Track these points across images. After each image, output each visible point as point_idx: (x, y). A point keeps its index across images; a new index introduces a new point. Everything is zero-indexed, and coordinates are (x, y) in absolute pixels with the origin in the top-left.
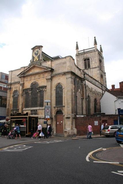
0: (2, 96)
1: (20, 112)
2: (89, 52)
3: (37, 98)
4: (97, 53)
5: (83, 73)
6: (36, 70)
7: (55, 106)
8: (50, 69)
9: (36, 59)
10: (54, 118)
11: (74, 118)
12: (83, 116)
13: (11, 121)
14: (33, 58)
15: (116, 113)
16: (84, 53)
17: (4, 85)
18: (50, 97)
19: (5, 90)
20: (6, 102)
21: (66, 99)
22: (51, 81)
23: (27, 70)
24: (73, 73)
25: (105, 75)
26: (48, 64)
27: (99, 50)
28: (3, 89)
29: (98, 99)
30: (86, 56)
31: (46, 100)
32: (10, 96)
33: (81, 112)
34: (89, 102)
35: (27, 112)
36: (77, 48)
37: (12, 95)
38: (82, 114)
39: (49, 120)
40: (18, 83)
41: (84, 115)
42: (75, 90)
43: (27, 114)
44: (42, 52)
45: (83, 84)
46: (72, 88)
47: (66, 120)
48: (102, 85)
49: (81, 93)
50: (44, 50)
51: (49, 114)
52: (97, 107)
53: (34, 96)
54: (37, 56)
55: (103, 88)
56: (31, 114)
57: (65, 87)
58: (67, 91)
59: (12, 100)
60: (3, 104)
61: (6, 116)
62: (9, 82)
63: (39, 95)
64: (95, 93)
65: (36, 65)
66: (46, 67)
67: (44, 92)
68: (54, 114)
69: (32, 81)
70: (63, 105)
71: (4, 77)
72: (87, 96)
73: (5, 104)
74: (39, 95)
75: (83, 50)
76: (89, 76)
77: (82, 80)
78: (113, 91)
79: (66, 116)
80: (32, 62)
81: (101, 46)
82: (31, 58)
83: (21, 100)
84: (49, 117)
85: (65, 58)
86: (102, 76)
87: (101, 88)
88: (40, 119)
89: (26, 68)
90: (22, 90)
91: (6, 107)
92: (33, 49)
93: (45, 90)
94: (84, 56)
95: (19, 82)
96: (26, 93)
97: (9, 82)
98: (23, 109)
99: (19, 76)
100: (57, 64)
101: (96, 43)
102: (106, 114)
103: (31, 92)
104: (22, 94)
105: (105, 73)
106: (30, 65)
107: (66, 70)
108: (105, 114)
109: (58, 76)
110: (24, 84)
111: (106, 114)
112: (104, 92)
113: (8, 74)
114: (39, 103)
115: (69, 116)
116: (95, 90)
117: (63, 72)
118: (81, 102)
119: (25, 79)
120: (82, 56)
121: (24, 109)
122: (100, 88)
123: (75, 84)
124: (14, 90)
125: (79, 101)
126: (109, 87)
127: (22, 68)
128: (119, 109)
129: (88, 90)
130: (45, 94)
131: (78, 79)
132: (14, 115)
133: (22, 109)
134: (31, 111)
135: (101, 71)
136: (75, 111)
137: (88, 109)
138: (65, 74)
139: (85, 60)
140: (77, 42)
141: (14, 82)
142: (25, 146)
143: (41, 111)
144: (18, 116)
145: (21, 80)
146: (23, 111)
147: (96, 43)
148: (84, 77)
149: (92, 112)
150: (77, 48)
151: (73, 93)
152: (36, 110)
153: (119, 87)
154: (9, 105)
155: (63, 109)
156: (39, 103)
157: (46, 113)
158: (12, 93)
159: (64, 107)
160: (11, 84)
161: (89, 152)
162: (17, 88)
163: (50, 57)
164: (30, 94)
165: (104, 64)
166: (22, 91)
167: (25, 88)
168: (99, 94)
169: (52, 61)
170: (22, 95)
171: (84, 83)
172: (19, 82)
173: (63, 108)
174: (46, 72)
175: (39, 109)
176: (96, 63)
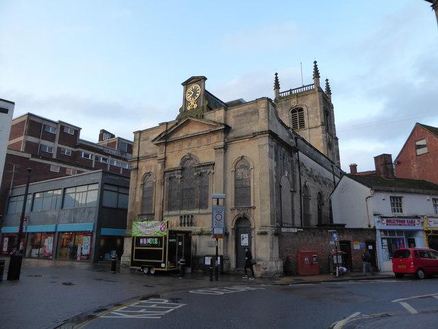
10: (230, 234)
12: (296, 230)
14: (186, 102)
25: (337, 144)
27: (324, 90)
28: (121, 173)
29: (326, 190)
34: (305, 198)
38: (294, 227)
41: (298, 228)
51: (222, 224)
52: (323, 211)
53: (187, 186)
66: (214, 122)
69: (184, 153)
70: (252, 205)
77: (292, 150)
78: (354, 175)
79: (257, 230)
80: (183, 111)
82: (180, 104)
85: (257, 101)
87: (331, 169)
89: (170, 126)
92: (187, 84)
101: (316, 74)
106: (179, 118)
110: (165, 158)
112: (337, 179)
118: (290, 199)
123: (276, 159)
127: (161, 124)
129: (304, 173)
137: (305, 217)
143: (202, 217)
145: (161, 150)
147: (316, 74)
149: (314, 221)
153: (374, 169)
159: (254, 208)
165: (334, 120)
167: (167, 169)
174: (214, 132)
175: (199, 214)
176: (317, 117)
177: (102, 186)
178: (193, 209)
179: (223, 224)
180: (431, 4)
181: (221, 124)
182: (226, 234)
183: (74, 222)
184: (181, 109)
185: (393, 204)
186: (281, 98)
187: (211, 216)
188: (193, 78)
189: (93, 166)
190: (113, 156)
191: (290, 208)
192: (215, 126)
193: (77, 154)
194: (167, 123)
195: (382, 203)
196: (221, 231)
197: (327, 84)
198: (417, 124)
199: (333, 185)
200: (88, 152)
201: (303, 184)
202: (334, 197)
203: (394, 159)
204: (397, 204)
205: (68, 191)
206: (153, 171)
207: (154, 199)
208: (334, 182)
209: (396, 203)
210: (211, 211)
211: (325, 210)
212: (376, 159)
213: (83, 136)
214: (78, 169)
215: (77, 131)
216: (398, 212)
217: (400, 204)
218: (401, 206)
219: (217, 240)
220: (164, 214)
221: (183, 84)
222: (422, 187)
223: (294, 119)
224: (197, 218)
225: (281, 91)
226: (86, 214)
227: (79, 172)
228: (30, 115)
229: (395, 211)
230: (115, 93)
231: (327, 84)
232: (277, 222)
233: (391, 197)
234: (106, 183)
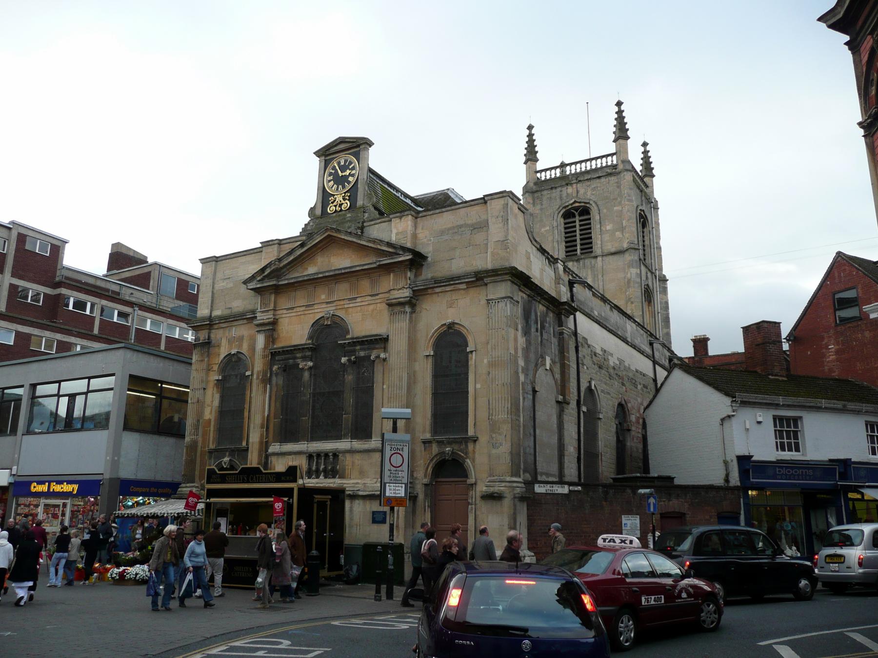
0: (162, 382)
1: (255, 465)
2: (587, 177)
3: (339, 394)
4: (628, 176)
5: (566, 278)
6: (341, 261)
7: (428, 436)
8: (409, 257)
9: (341, 205)
10: (421, 497)
11: (522, 499)
12: (565, 490)
13: (208, 505)
14: (325, 196)
15: (727, 480)
16: (565, 180)
17: (172, 328)
18: (401, 395)
19: (179, 351)
20: (185, 414)
21: (482, 402)
22: (411, 313)
23: (291, 258)
24: (521, 279)
25: (664, 291)
26: (397, 230)
27: (639, 168)
28: (163, 347)
29: (636, 402)
30: (571, 194)
31: (387, 409)
32: (207, 382)
33: (554, 468)
34: (589, 421)
35: (295, 463)
36: (531, 154)
37: (215, 377)
38: (561, 482)
39: (399, 505)
40: (247, 317)
41: (570, 484)
42: (527, 359)
43: (291, 473)
44: (371, 171)
45: (566, 331)
46: (516, 349)
47: (483, 508)
48: (651, 335)
49: (558, 376)
50: (378, 160)
51: (404, 475)
52: (628, 444)
53: (328, 384)
54: (344, 187)
55: (657, 354)
56: (309, 474)
57: (479, 347)
58: (492, 364)
59: (216, 403)
60: (163, 417)
61: (178, 478)
62: (203, 311)
63: (349, 378)
64: (620, 375)
65: (338, 231)
66: (389, 244)
67: (378, 368)
68: (422, 477)
69: (320, 311)
70: (471, 432)
71: (172, 287)
72: (583, 389)
73: (176, 419)
74: (349, 378)
75: (558, 164)
76: (594, 295)
77: (562, 309)
78: (703, 365)
79: (482, 488)
80: (320, 214)
81: (648, 148)
82: (311, 198)
83: (260, 404)
84: (401, 492)
85: (484, 200)
86: (648, 295)
87: (648, 350)
88: (354, 497)
89: (287, 248)
90: (267, 352)
91: (183, 436)
92: (326, 154)
93: (382, 355)
94: (564, 194)
95: (253, 312)
96: (285, 371)
97: (203, 311)
98: (267, 450)
99: (252, 285)
100: (442, 232)
101: (622, 132)
102: (677, 482)
103: (310, 364)
104: (264, 373)
105: (664, 280)
106: (307, 232)
107: (486, 262)
108: (671, 479)
109: (448, 288)
110: (274, 323)
111: (677, 482)
112: (661, 374)
113: (198, 274)
114: (347, 418)
115: (497, 488)
116: (621, 361)
117: (470, 268)
118: (554, 419)
119: (284, 302)
120: (556, 193)
121: (274, 448)
122: (642, 352)
123: (526, 333)
124: (223, 352)
125: (547, 413)
126: (684, 349)
127: (266, 244)
128: (744, 461)
129: (587, 361)
130: (378, 377)
131: (541, 308)
132: (223, 479)
133: (264, 445)
134: (310, 457)
135: (643, 268)
136: (525, 462)
137: (588, 456)
138: (482, 279)
139: (568, 215)
140: (530, 128)
141: (227, 312)
142: (285, 644)
143: (357, 459)
144: (248, 482)
145: (263, 304)
146: (267, 457)
147: (622, 132)
148: (572, 296)
149: (607, 468)
150: (531, 154)
151: (517, 373)
152: (335, 455)
153: (741, 349)
154: (196, 427)
155: (470, 455)
156: (347, 418)
157: (387, 473)
158: (216, 368)
159: (475, 440)
160: (210, 323)
161: (451, 580)
162: (240, 346)
163: (407, 196)
164: (306, 375)
165: (658, 237)
166: (264, 357)
167: (279, 345)
168: (639, 379)
169: (417, 215)
170: (266, 380)
171: (572, 326)
172: (253, 312)
173: (471, 446)
174: (387, 269)
175: (351, 452)
176: (622, 229)
178: (338, 437)
179: (405, 474)
180: (847, 38)
181: (405, 249)
182: (413, 498)
184: (312, 211)
185: (779, 434)
186: (539, 182)
187: (377, 456)
188: (341, 141)
190: (144, 308)
191: (555, 440)
192: (391, 254)
193: (55, 304)
194: (280, 242)
195: (754, 435)
196: (400, 492)
197: (646, 152)
198: (839, 254)
199: (651, 385)
200: (82, 297)
201: (584, 386)
202: (654, 416)
203: (785, 331)
204: (788, 432)
205: (41, 390)
206: (245, 349)
207: (246, 414)
208: (655, 380)
209: (788, 432)
210: (379, 445)
211: (633, 443)
212: (746, 330)
213: (71, 259)
214: (59, 336)
215: (57, 247)
216: (790, 450)
217: (796, 434)
218: (796, 437)
219: (392, 509)
220: (271, 450)
221: (318, 153)
222: (845, 393)
223: (569, 232)
224: (347, 461)
225: (540, 166)
227: (63, 347)
229: (783, 449)
230: (183, 186)
231: (646, 152)
232: (525, 471)
233: (775, 418)
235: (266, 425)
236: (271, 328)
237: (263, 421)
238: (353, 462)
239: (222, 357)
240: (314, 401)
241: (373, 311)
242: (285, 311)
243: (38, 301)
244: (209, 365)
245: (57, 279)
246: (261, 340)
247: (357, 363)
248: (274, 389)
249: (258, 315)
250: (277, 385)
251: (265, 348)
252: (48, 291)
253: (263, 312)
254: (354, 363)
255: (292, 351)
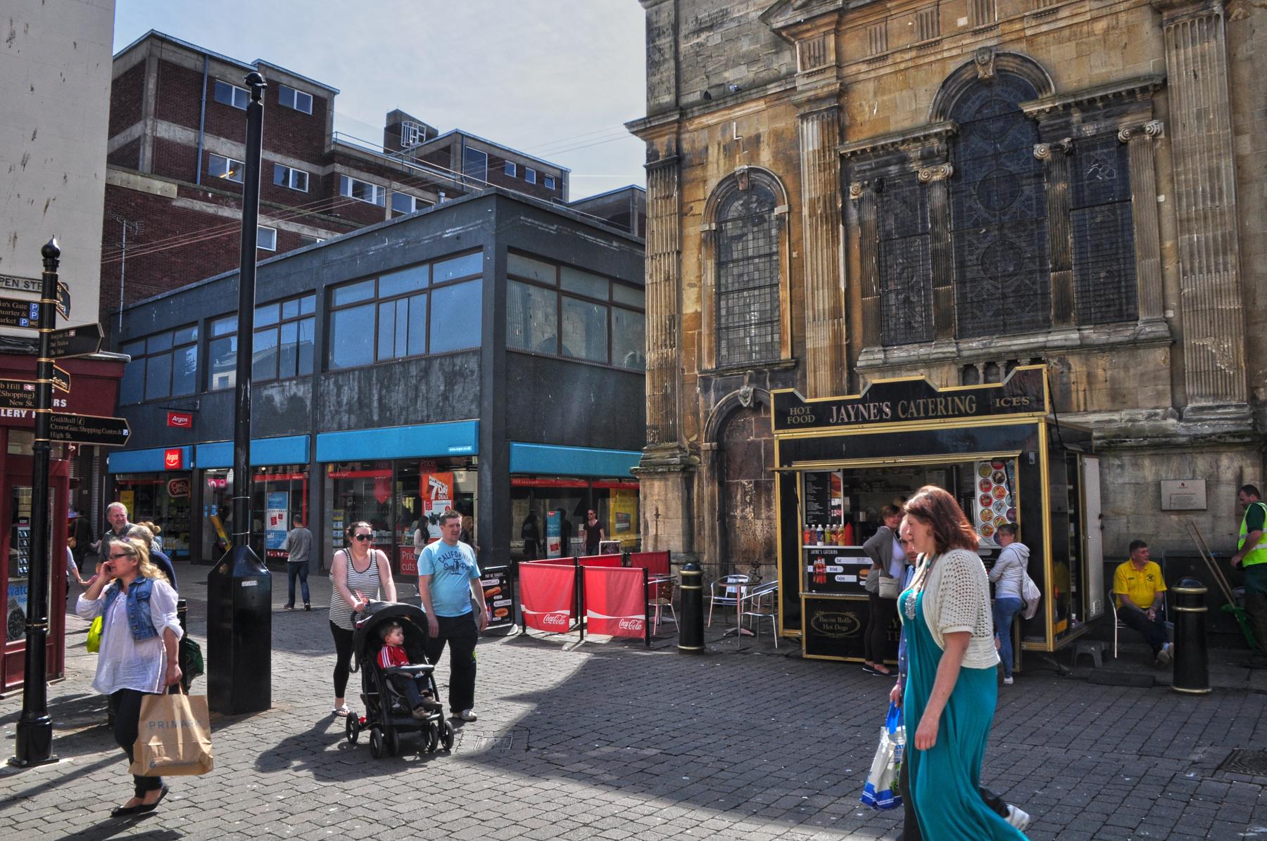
32: (681, 238)
37: (696, 229)
74: (1060, 188)
124: (715, 172)
158: (700, 208)
162: (754, 156)
164: (938, 195)
170: (835, 216)
175: (1085, 349)
177: (500, 265)
178: (1044, 326)
183: (390, 422)
189: (376, 418)
200: (364, 177)
215: (323, 100)
226: (438, 381)
228: (153, 37)
234: (512, 250)
235: (843, 312)
236: (835, 111)
237: (837, 301)
238: (1090, 377)
239: (712, 183)
240: (960, 249)
241: (1107, 32)
242: (864, 67)
243: (304, 188)
244: (681, 204)
245: (327, 150)
246: (811, 134)
247: (1073, 156)
248: (856, 234)
249: (800, 83)
250: (861, 223)
251: (824, 149)
252: (319, 170)
253: (810, 75)
254: (1070, 153)
255: (888, 152)
